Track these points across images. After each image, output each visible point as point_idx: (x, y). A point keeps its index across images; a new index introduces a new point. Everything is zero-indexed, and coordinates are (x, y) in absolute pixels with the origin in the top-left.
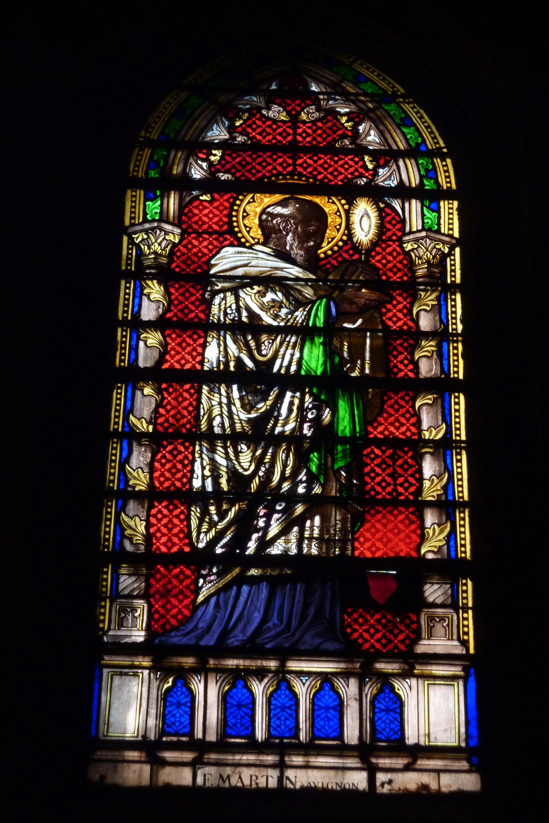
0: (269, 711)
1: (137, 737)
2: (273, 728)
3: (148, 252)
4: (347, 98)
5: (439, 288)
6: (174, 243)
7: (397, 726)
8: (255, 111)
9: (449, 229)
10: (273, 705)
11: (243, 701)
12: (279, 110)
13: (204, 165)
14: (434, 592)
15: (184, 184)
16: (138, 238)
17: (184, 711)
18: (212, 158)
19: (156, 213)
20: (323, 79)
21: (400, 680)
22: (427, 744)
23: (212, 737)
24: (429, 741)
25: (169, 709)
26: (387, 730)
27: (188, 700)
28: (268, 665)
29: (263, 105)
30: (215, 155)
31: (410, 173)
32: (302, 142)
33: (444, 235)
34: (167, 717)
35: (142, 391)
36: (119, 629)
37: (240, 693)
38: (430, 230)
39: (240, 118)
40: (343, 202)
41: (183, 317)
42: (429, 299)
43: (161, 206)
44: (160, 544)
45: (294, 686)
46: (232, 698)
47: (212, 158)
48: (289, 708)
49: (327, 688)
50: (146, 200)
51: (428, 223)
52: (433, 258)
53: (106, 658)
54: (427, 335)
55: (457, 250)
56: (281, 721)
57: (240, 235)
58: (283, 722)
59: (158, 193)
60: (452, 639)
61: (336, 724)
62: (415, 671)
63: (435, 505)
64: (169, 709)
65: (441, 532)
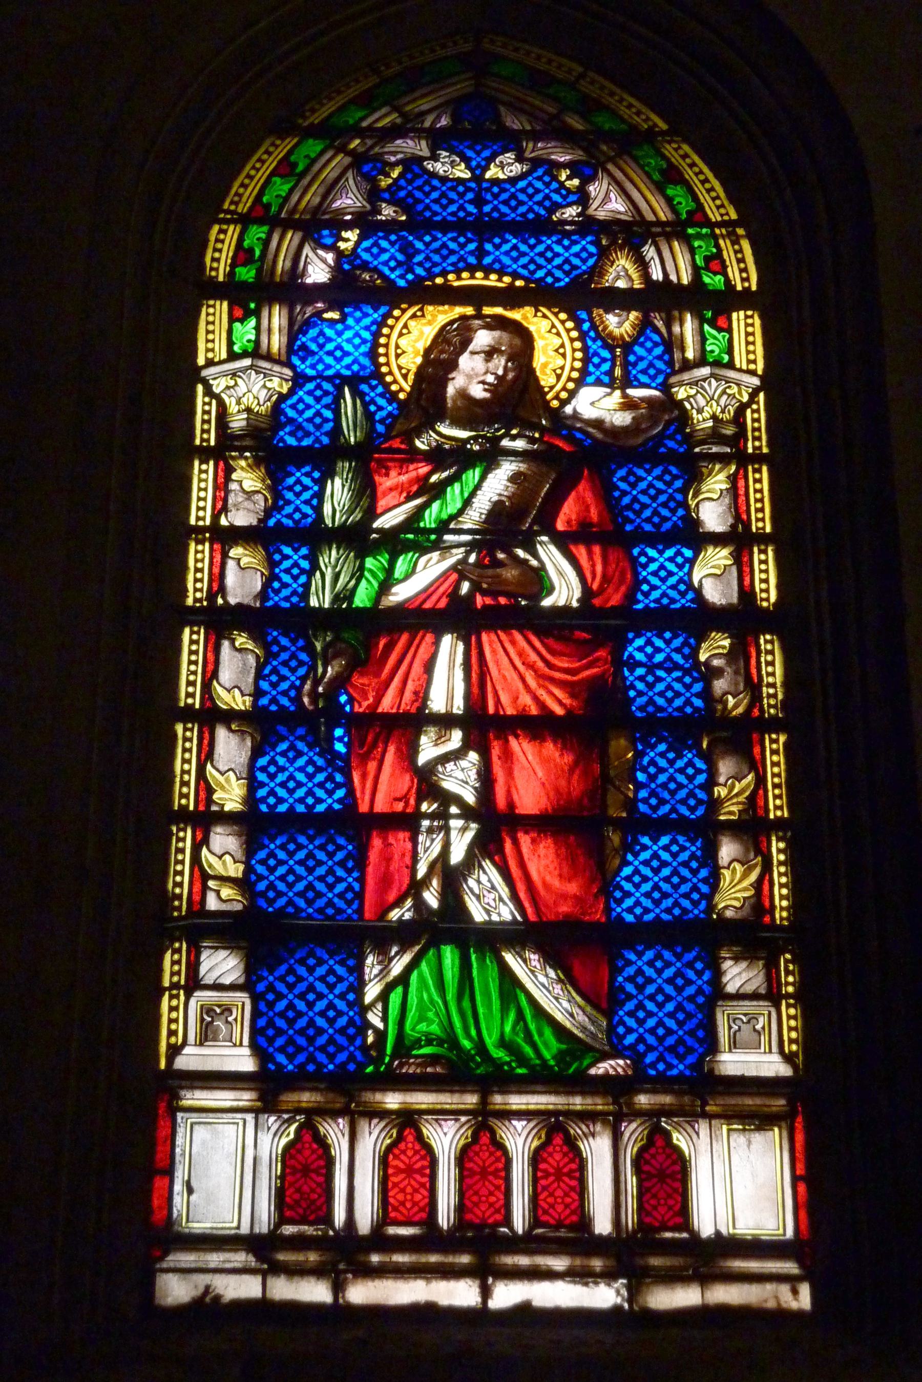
0: (535, 1180)
1: (238, 1227)
2: (393, 1206)
3: (235, 411)
4: (566, 137)
5: (207, 535)
6: (280, 393)
7: (424, 1197)
8: (412, 164)
9: (749, 362)
10: (542, 1171)
11: (312, 1163)
12: (453, 161)
13: (330, 257)
14: (738, 975)
15: (290, 290)
16: (218, 386)
17: (494, 1185)
18: (342, 245)
19: (249, 341)
20: (526, 107)
21: (330, 1121)
22: (731, 1231)
23: (364, 1222)
24: (734, 1227)
25: (543, 1182)
26: (408, 1205)
27: (426, 1163)
28: (589, 1101)
29: (426, 153)
30: (347, 240)
31: (675, 265)
32: (380, 238)
33: (740, 370)
34: (542, 1196)
35: (233, 641)
36: (201, 1044)
37: (409, 1153)
38: (717, 364)
39: (387, 175)
40: (563, 316)
41: (635, 469)
42: (717, 482)
43: (258, 328)
44: (690, 880)
45: (501, 1137)
46: (647, 1162)
47: (342, 245)
48: (569, 1174)
49: (410, 1138)
50: (232, 320)
51: (712, 352)
52: (723, 412)
53: (189, 1095)
54: (717, 539)
55: (762, 396)
56: (406, 1194)
57: (389, 379)
58: (409, 1197)
59: (252, 306)
60: (770, 1052)
61: (424, 1197)
62: (707, 1108)
63: (735, 829)
64: (543, 1182)
65: (745, 875)
